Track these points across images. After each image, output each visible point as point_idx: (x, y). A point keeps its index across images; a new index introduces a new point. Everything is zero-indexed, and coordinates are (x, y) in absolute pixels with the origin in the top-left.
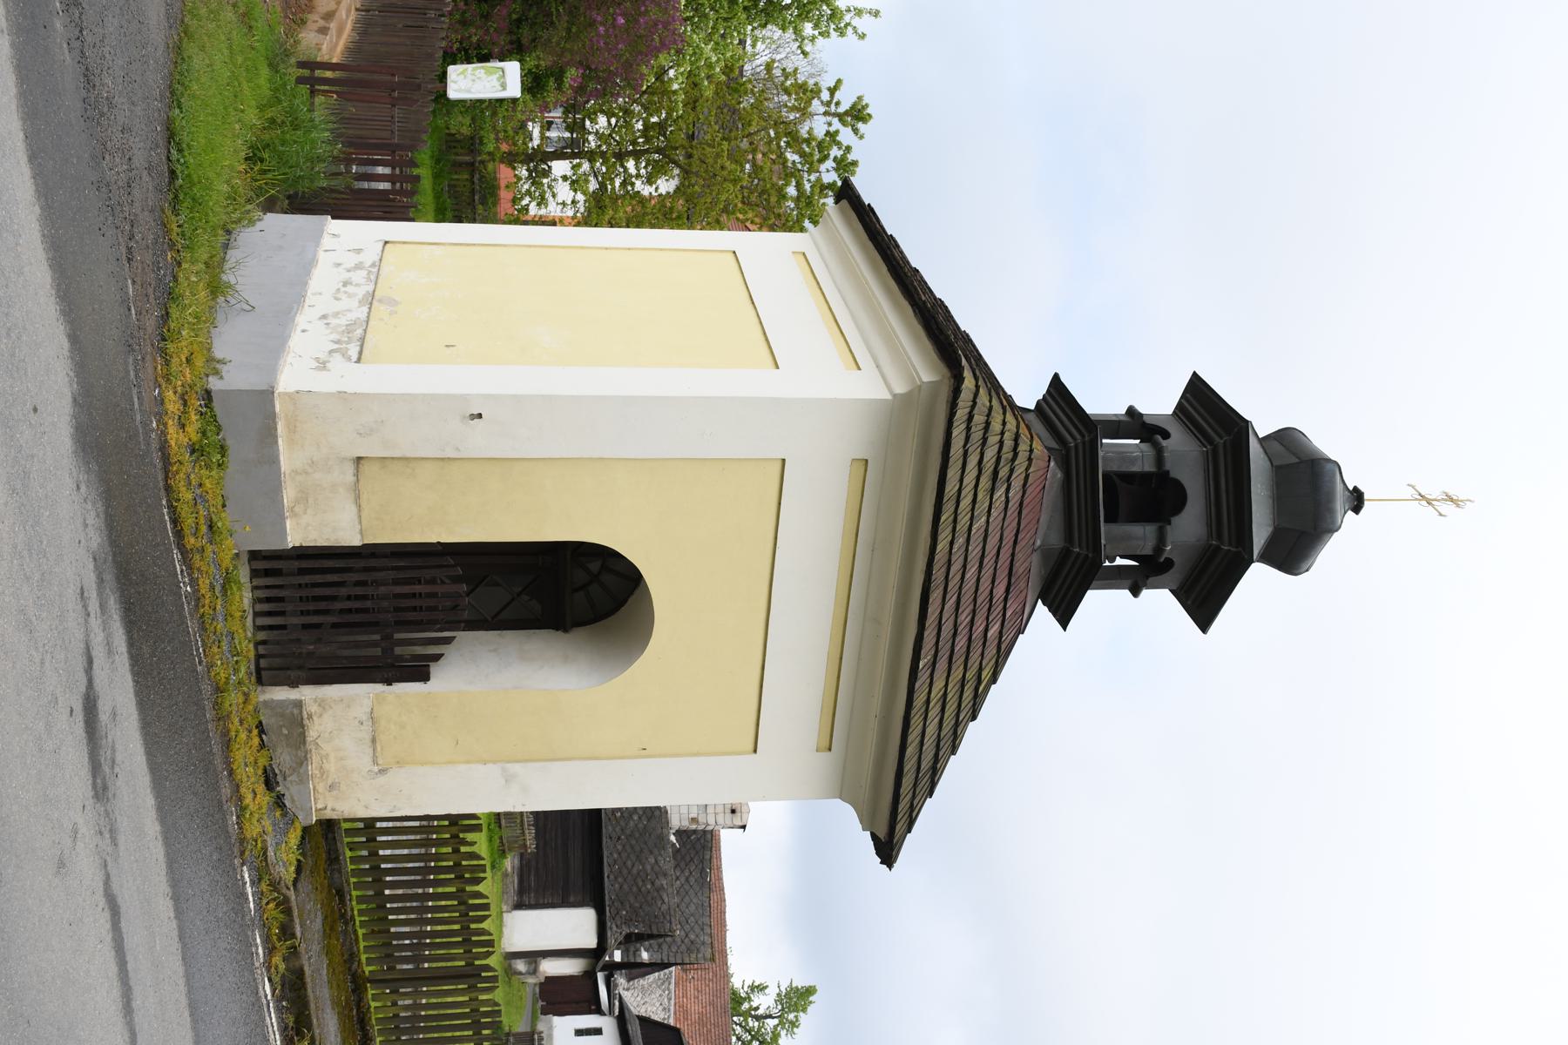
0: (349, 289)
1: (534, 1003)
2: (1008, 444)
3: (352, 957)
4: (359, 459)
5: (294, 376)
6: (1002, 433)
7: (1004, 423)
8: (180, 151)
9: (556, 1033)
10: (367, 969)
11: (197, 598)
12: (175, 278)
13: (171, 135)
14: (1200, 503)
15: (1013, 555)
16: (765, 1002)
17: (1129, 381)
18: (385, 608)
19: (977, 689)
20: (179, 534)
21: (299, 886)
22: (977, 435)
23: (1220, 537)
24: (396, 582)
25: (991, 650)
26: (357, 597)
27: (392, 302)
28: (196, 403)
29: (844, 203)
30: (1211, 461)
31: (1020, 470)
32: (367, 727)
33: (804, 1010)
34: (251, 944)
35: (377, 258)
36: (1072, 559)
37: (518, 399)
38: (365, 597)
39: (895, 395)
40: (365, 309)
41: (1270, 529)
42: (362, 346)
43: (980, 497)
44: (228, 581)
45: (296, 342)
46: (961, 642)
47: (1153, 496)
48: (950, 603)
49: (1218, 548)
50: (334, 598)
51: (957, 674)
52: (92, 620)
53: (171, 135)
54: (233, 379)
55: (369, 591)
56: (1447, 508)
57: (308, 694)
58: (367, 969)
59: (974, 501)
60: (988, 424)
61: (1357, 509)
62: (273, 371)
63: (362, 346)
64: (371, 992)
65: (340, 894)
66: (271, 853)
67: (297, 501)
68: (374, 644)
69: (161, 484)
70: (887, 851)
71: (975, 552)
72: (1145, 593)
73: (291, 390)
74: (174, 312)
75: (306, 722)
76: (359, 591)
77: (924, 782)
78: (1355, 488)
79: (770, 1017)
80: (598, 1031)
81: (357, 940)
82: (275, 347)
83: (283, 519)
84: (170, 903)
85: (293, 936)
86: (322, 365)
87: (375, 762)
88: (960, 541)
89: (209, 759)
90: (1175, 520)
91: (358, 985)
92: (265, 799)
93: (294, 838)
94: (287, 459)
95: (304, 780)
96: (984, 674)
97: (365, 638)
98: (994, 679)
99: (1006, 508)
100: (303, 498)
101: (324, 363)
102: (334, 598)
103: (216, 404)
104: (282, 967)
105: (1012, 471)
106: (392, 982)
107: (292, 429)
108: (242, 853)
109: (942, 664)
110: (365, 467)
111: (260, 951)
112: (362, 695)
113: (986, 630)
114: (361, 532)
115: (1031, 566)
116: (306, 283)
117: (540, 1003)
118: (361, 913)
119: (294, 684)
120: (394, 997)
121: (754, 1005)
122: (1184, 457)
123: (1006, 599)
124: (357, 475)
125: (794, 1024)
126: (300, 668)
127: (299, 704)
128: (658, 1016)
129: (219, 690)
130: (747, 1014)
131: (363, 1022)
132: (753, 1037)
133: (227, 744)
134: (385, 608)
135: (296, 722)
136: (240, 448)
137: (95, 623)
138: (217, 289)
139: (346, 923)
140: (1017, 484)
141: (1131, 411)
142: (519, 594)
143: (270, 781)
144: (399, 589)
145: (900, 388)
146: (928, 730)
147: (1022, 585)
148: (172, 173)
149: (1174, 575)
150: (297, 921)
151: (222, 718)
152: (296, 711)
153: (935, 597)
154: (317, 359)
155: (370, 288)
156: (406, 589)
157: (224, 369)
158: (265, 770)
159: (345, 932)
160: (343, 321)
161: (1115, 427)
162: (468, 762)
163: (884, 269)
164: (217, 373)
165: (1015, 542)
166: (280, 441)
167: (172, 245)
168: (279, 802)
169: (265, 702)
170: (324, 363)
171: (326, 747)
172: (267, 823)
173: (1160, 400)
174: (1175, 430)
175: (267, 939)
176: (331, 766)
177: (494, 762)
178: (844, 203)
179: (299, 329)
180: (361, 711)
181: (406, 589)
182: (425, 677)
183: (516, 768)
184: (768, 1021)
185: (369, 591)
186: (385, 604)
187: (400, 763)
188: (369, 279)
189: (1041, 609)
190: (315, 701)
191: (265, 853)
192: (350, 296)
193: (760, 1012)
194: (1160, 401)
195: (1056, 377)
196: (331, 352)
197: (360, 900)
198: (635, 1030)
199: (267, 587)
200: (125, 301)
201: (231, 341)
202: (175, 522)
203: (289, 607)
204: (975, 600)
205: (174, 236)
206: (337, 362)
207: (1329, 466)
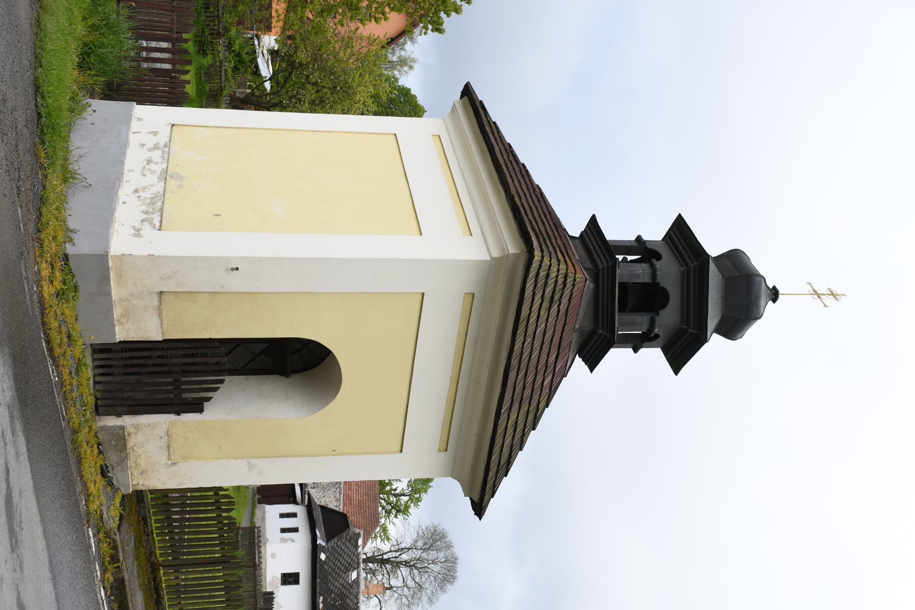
0: (152, 166)
1: (254, 495)
2: (560, 281)
3: (151, 553)
4: (161, 293)
5: (120, 243)
6: (557, 276)
7: (558, 270)
8: (43, 97)
9: (267, 516)
10: (160, 559)
11: (62, 383)
12: (44, 187)
13: (37, 89)
14: (680, 296)
15: (561, 338)
16: (401, 486)
17: (635, 220)
18: (173, 374)
19: (536, 414)
20: (51, 350)
21: (122, 529)
22: (541, 282)
23: (688, 324)
24: (184, 356)
25: (546, 391)
26: (158, 365)
27: (180, 178)
28: (59, 264)
29: (466, 98)
30: (686, 277)
31: (567, 292)
32: (165, 439)
33: (426, 492)
34: (93, 571)
35: (167, 140)
36: (596, 337)
37: (261, 260)
38: (163, 365)
39: (492, 258)
40: (162, 184)
41: (719, 318)
42: (161, 216)
43: (542, 314)
44: (79, 365)
45: (121, 212)
46: (528, 392)
47: (649, 298)
48: (522, 374)
49: (686, 331)
50: (144, 365)
51: (524, 409)
52: (9, 445)
53: (37, 89)
54: (80, 246)
55: (166, 361)
56: (829, 300)
57: (128, 421)
58: (160, 559)
59: (538, 317)
60: (548, 274)
61: (774, 300)
62: (105, 239)
63: (161, 216)
64: (162, 572)
65: (145, 519)
66: (105, 515)
67: (123, 316)
68: (170, 392)
69: (40, 321)
70: (479, 509)
71: (537, 343)
72: (642, 351)
73: (119, 253)
74: (44, 211)
75: (127, 437)
76: (160, 361)
77: (503, 470)
78: (774, 288)
79: (404, 495)
80: (296, 530)
81: (154, 543)
82: (106, 219)
83: (113, 326)
84: (51, 584)
85: (118, 561)
86: (137, 233)
87: (169, 459)
88: (529, 340)
89: (66, 459)
90: (661, 312)
91: (154, 568)
92: (101, 482)
93: (118, 501)
94: (116, 292)
95: (125, 469)
96: (541, 406)
97: (162, 380)
98: (547, 405)
99: (558, 315)
100: (126, 314)
101: (138, 230)
102: (144, 365)
103: (71, 262)
104: (111, 579)
105: (562, 295)
106: (177, 566)
107: (119, 276)
108: (88, 521)
109: (516, 406)
110: (165, 297)
111: (99, 573)
112: (161, 421)
113: (543, 381)
114: (162, 333)
115: (572, 339)
116: (123, 163)
117: (258, 496)
118: (157, 528)
119: (119, 415)
120: (177, 574)
121: (394, 487)
122: (668, 272)
123: (556, 362)
124: (160, 301)
125: (418, 500)
126: (122, 405)
127: (122, 428)
128: (332, 506)
129: (75, 432)
130: (389, 493)
131: (157, 589)
132: (393, 507)
133: (79, 461)
134: (173, 374)
135: (120, 438)
136: (86, 287)
137: (10, 447)
138: (68, 176)
139: (148, 535)
140: (565, 301)
141: (639, 239)
142: (259, 355)
143: (104, 472)
144: (184, 360)
145: (496, 254)
146: (506, 444)
147: (566, 351)
148: (39, 115)
149: (660, 341)
150: (120, 551)
151: (77, 448)
152: (120, 432)
153: (512, 374)
154: (134, 227)
155: (164, 166)
156: (190, 360)
157: (75, 237)
158: (101, 467)
159: (147, 541)
160: (147, 195)
161: (625, 248)
162: (227, 458)
163: (490, 159)
164: (71, 240)
165: (563, 331)
166: (112, 283)
167: (42, 167)
168: (110, 483)
169: (101, 427)
170: (138, 230)
171: (139, 451)
172: (103, 498)
173: (655, 232)
174: (665, 252)
175: (102, 565)
176: (142, 461)
177: (243, 458)
178: (466, 98)
179: (121, 201)
180: (161, 431)
181: (190, 360)
182: (200, 410)
183: (256, 461)
184: (403, 497)
185: (166, 361)
186: (176, 369)
187: (185, 459)
188: (163, 157)
189: (578, 360)
190: (133, 425)
191: (102, 517)
192: (152, 172)
193: (397, 492)
194: (655, 233)
195: (593, 220)
196: (142, 221)
197: (156, 521)
198: (318, 515)
199: (101, 359)
200: (17, 221)
201: (78, 211)
202: (48, 342)
203: (116, 371)
204: (537, 368)
205: (43, 161)
206: (146, 229)
207: (758, 279)
